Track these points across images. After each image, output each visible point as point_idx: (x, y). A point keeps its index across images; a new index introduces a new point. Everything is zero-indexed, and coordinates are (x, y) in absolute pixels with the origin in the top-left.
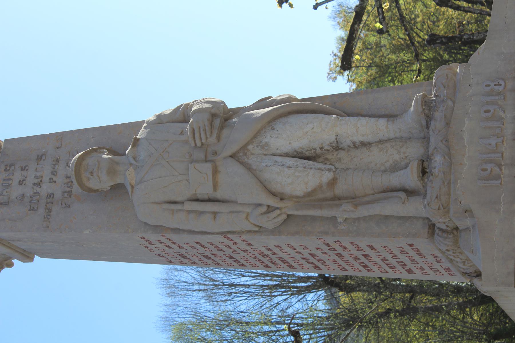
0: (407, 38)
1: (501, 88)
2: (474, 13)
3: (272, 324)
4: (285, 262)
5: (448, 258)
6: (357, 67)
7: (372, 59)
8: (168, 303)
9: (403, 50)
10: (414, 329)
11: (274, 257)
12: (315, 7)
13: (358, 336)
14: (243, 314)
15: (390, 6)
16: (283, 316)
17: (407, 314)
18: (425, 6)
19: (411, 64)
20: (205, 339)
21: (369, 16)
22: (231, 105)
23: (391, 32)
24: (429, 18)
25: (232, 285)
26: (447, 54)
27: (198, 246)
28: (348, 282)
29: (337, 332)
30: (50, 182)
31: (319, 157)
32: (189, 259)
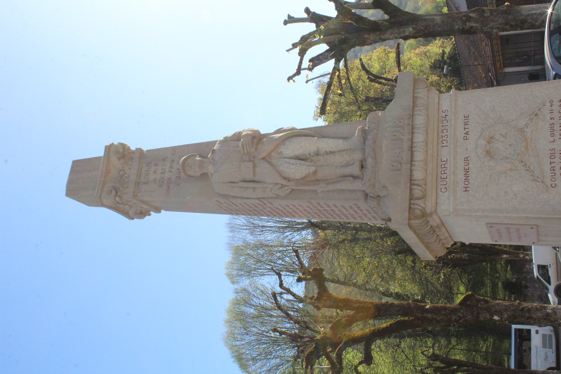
0: (355, 99)
1: (402, 124)
2: (389, 86)
3: (284, 246)
4: (290, 214)
5: (374, 211)
6: (328, 113)
7: (336, 109)
8: (230, 235)
9: (352, 105)
10: (357, 250)
11: (285, 211)
12: (307, 82)
13: (328, 253)
14: (269, 242)
15: (346, 82)
16: (290, 243)
17: (354, 241)
18: (364, 82)
19: (357, 112)
20: (249, 254)
21: (335, 87)
22: (262, 132)
23: (346, 95)
24: (366, 88)
25: (263, 227)
26: (375, 107)
27: (245, 205)
28: (323, 225)
29: (318, 251)
30: (169, 172)
31: (308, 159)
32: (241, 212)
